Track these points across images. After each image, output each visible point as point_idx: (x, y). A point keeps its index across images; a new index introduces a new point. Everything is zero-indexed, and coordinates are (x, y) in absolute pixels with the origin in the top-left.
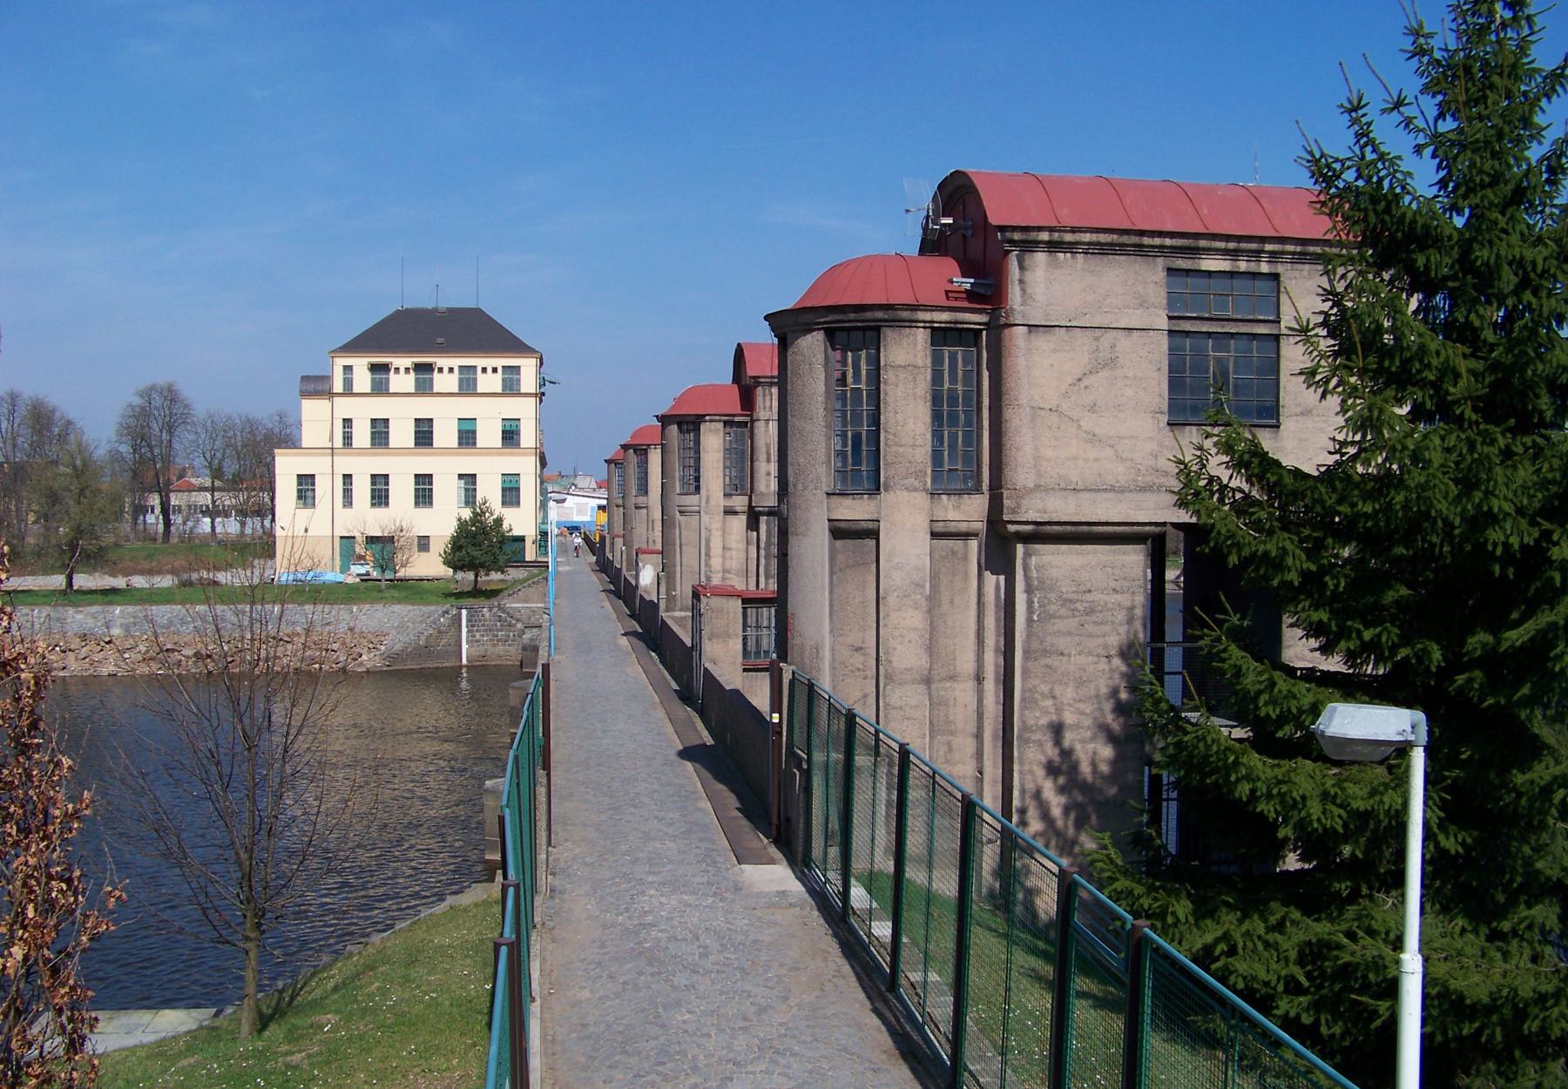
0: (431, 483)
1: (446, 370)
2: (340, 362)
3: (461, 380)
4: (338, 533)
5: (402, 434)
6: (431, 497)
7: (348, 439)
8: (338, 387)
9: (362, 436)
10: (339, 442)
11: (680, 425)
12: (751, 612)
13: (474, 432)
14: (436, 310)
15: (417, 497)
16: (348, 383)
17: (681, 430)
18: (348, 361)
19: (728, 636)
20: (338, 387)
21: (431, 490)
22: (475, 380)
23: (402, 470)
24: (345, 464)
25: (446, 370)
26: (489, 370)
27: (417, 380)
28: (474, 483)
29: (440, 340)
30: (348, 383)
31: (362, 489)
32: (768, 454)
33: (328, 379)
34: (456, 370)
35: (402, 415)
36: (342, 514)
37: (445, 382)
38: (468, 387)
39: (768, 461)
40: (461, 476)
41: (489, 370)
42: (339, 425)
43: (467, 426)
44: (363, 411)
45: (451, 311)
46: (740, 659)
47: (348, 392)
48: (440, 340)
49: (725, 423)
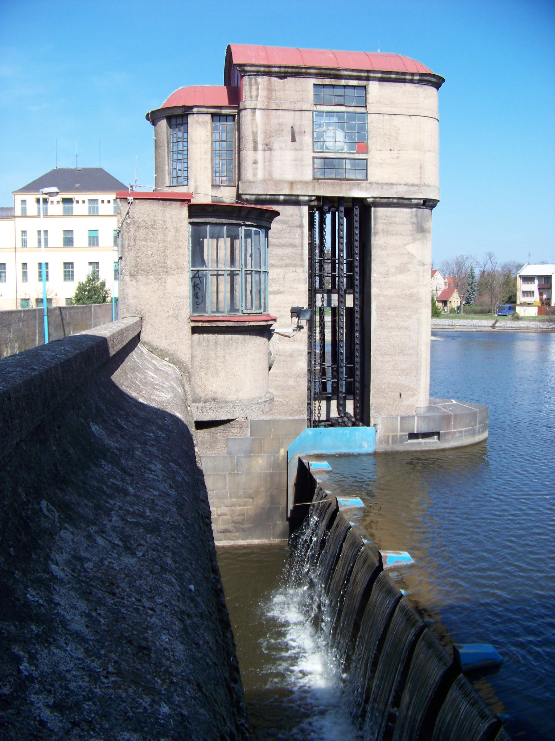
0: (73, 268)
1: (80, 202)
2: (19, 198)
3: (90, 208)
4: (19, 297)
5: (56, 239)
6: (73, 275)
7: (24, 243)
8: (18, 212)
9: (32, 240)
10: (19, 244)
11: (169, 119)
12: (217, 249)
13: (97, 238)
14: (76, 169)
15: (65, 276)
16: (24, 210)
17: (170, 125)
18: (24, 197)
19: (165, 270)
20: (18, 212)
21: (73, 272)
22: (97, 208)
23: (56, 260)
24: (23, 256)
25: (80, 202)
26: (106, 202)
27: (64, 208)
28: (98, 267)
29: (77, 185)
30: (24, 210)
31: (33, 271)
32: (255, 143)
33: (12, 209)
34: (87, 202)
35: (56, 228)
36: (22, 285)
37: (79, 209)
38: (93, 213)
39: (255, 149)
40: (90, 263)
41: (106, 202)
42: (19, 234)
43: (93, 234)
44: (32, 226)
45: (84, 169)
46: (186, 309)
47: (24, 215)
48: (77, 185)
49: (213, 115)
